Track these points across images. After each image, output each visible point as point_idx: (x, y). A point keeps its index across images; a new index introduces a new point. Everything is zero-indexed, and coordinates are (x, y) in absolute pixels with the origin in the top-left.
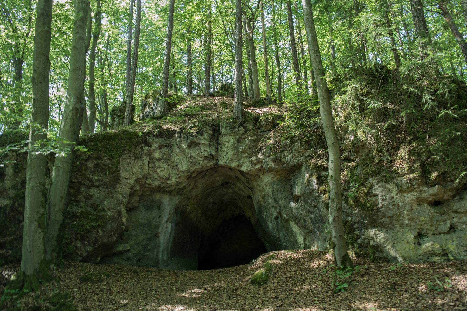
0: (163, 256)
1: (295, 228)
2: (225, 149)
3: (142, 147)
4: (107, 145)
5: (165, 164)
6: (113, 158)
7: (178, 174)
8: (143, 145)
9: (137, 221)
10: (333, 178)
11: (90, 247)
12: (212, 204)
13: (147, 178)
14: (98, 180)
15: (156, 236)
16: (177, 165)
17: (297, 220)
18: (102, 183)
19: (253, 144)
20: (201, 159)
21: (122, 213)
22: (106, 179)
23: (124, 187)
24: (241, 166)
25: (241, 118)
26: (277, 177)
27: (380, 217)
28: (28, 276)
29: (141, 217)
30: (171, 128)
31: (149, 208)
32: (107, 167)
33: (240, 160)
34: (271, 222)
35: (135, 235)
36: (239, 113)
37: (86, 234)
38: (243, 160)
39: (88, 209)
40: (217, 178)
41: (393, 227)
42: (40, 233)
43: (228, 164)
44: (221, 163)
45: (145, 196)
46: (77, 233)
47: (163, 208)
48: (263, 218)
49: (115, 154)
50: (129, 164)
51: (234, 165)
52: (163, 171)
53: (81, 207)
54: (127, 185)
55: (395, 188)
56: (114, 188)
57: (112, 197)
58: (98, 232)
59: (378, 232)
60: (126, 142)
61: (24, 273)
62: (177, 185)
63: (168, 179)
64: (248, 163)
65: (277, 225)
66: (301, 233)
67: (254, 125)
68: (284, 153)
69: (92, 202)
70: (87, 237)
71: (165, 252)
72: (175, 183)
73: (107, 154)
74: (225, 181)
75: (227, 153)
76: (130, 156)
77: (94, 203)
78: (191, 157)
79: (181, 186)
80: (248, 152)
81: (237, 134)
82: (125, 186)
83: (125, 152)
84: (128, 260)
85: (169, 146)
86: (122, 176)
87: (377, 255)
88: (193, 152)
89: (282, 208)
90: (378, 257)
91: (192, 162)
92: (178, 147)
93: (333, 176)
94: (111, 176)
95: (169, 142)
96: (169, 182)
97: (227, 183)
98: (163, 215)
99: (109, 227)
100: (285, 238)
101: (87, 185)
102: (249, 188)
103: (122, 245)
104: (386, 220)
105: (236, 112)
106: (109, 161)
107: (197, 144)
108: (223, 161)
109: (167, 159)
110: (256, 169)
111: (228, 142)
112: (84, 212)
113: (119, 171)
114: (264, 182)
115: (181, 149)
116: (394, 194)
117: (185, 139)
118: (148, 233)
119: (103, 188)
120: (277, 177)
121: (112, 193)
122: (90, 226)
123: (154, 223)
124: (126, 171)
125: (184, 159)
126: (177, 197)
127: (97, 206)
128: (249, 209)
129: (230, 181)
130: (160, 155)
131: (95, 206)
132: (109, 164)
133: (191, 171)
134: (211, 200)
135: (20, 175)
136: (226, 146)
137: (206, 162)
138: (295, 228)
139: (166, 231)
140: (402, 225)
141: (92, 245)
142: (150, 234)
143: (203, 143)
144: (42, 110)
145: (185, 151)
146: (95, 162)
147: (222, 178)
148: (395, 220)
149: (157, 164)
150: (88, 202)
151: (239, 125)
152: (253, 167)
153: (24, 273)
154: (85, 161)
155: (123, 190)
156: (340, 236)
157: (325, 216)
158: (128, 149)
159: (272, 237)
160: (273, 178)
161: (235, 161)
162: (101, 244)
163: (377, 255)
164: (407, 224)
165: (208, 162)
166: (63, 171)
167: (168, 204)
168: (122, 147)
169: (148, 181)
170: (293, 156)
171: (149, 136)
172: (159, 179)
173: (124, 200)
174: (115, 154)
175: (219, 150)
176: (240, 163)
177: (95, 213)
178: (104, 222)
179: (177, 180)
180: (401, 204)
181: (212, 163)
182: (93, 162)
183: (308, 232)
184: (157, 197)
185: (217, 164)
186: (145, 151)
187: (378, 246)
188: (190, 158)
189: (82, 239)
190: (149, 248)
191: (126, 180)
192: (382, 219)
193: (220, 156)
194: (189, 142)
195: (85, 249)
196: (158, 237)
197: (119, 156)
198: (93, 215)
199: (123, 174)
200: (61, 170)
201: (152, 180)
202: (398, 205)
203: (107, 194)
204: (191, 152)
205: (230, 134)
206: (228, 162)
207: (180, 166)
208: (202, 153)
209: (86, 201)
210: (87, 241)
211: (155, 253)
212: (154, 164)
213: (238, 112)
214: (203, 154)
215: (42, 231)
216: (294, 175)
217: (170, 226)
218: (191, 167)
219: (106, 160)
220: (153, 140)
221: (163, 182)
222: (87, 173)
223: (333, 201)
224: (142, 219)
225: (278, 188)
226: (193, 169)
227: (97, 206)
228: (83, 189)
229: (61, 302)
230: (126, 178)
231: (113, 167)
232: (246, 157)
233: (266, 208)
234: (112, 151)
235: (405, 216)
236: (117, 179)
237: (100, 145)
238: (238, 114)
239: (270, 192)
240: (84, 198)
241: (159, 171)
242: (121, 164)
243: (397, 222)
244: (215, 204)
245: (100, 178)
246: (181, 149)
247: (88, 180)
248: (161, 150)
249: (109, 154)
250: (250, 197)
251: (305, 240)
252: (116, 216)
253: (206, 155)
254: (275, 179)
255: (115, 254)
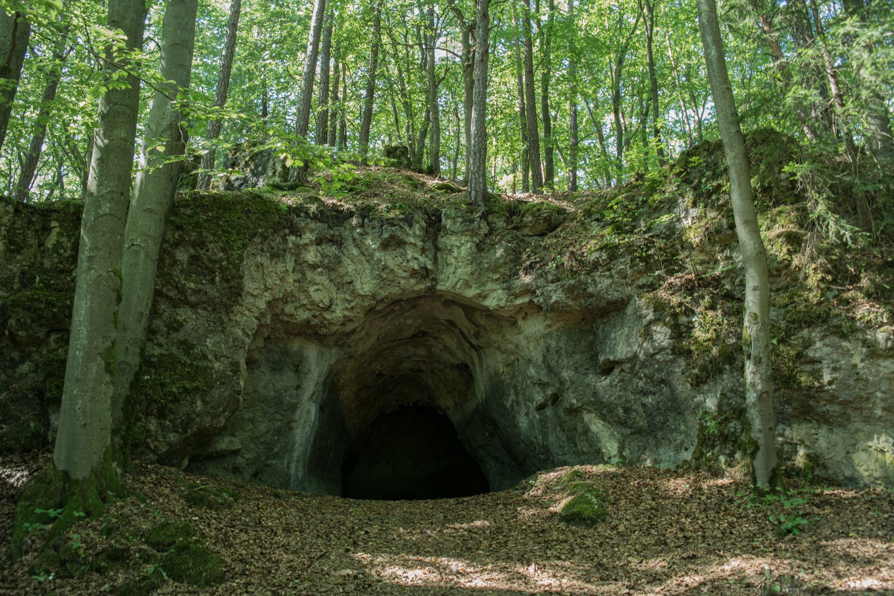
0: (297, 470)
1: (597, 426)
2: (453, 260)
3: (285, 235)
4: (218, 218)
5: (325, 277)
6: (231, 248)
7: (350, 302)
8: (287, 231)
9: (255, 391)
10: (759, 319)
11: (176, 435)
12: (374, 377)
13: (286, 302)
14: (196, 292)
15: (288, 427)
16: (351, 283)
17: (605, 411)
18: (204, 299)
19: (512, 257)
20: (405, 275)
21: (241, 368)
22: (213, 292)
23: (247, 312)
24: (485, 298)
25: (481, 203)
26: (558, 324)
27: (822, 403)
28: (77, 480)
29: (262, 383)
30: (341, 206)
31: (276, 367)
32: (217, 266)
33: (484, 284)
34: (527, 414)
35: (252, 420)
36: (479, 194)
37: (170, 405)
38: (490, 286)
39: (174, 350)
40: (409, 322)
41: (846, 423)
42: (107, 384)
43: (458, 291)
44: (443, 288)
45: (281, 337)
46: (152, 401)
47: (306, 370)
48: (505, 408)
49: (235, 241)
50: (260, 266)
51: (471, 293)
52: (320, 290)
53: (160, 345)
54: (254, 309)
55: (859, 349)
56: (227, 313)
57: (223, 331)
58: (193, 402)
59: (813, 431)
60: (258, 218)
61: (66, 474)
62: (343, 324)
63: (328, 308)
64: (500, 292)
65: (541, 420)
66: (612, 435)
67: (508, 221)
68: (593, 276)
69: (180, 336)
70: (171, 411)
71: (301, 464)
72: (341, 319)
73: (220, 238)
74: (423, 329)
75: (456, 268)
76: (262, 250)
77: (186, 340)
78: (385, 267)
79: (350, 327)
80: (501, 270)
81: (476, 235)
82: (249, 310)
83: (255, 239)
84: (234, 473)
85: (338, 242)
86: (246, 289)
87: (817, 472)
88: (390, 259)
89: (567, 386)
90: (818, 476)
91: (384, 279)
92: (357, 246)
93: (758, 314)
94: (226, 285)
95: (337, 233)
96: (328, 316)
97: (424, 334)
98: (305, 385)
99: (216, 393)
100: (560, 446)
101: (172, 298)
102: (473, 346)
103: (227, 439)
104: (835, 408)
105: (473, 193)
106: (221, 254)
107: (401, 244)
108: (448, 285)
109: (331, 267)
110: (514, 306)
111: (459, 248)
112: (165, 356)
113: (241, 277)
114: (525, 333)
115: (363, 249)
116: (856, 360)
117: (376, 230)
118: (275, 419)
119: (205, 309)
120: (558, 324)
121: (222, 323)
122: (178, 388)
123: (287, 398)
124: (253, 280)
125: (367, 271)
126: (334, 350)
127: (192, 347)
128: (448, 393)
129: (431, 331)
130: (316, 256)
131: (187, 346)
132: (221, 260)
133: (379, 298)
134: (378, 367)
135: (18, 257)
136: (455, 254)
137: (413, 281)
138: (597, 426)
139: (306, 418)
140: (867, 420)
141: (180, 430)
142: (280, 420)
143: (411, 243)
144: (128, 111)
145: (372, 256)
146: (192, 252)
147: (420, 321)
148: (856, 409)
149: (309, 275)
150: (174, 335)
151: (481, 218)
152: (511, 301)
153: (66, 474)
154: (171, 246)
155: (246, 317)
156: (770, 429)
157: (686, 400)
158: (262, 234)
159: (522, 446)
160: (550, 326)
161: (474, 286)
162: (198, 429)
163: (817, 472)
164: (880, 417)
165: (417, 283)
166: (147, 255)
167: (316, 362)
168: (248, 228)
169: (289, 309)
170: (613, 283)
171: (298, 216)
172: (309, 307)
173: (247, 341)
174: (235, 241)
175: (439, 261)
176: (483, 291)
177: (189, 362)
178: (206, 383)
179: (347, 313)
180: (871, 378)
181: (422, 287)
182: (187, 251)
183: (631, 434)
184: (295, 345)
185: (432, 289)
186: (291, 245)
187: (818, 457)
188: (383, 270)
189: (161, 415)
190: (276, 450)
191: (251, 300)
192: (825, 405)
193: (442, 273)
194: (386, 236)
195: (164, 437)
196: (291, 429)
197: (244, 245)
198: (184, 365)
199: (249, 286)
200: (142, 255)
201: (296, 308)
202: (867, 381)
203: (211, 323)
204: (388, 257)
205: (463, 233)
206: (458, 286)
207: (358, 285)
208: (408, 261)
209: (169, 333)
210: (171, 421)
211: (285, 462)
212: (304, 274)
213: (477, 192)
214: (411, 264)
215: (112, 382)
216: (605, 320)
217: (313, 409)
218: (381, 288)
219: (215, 250)
220: (307, 224)
221: (317, 314)
222: (175, 273)
223: (760, 362)
224: (264, 387)
225: (561, 344)
226: (383, 293)
227: (192, 347)
228: (163, 307)
229: (177, 541)
230: (252, 295)
231: (230, 266)
232: (497, 280)
233: (515, 387)
234: (230, 233)
235: (878, 401)
236: (236, 293)
237: (205, 217)
238: (476, 196)
239: (537, 355)
240: (166, 326)
241: (312, 289)
242: (245, 263)
243: (859, 412)
244: (384, 375)
245: (200, 286)
246: (363, 249)
247: (177, 288)
248: (319, 248)
249: (224, 239)
250: (465, 370)
251: (621, 448)
252: (229, 373)
253: (416, 267)
254: (554, 328)
255: (210, 458)
